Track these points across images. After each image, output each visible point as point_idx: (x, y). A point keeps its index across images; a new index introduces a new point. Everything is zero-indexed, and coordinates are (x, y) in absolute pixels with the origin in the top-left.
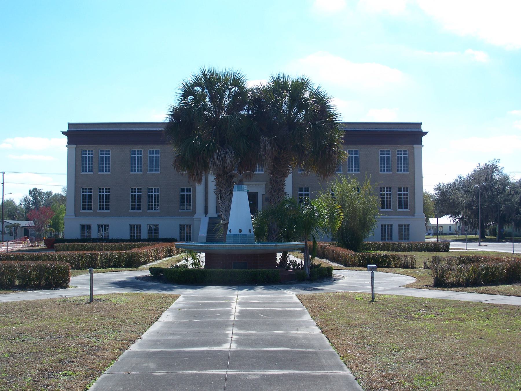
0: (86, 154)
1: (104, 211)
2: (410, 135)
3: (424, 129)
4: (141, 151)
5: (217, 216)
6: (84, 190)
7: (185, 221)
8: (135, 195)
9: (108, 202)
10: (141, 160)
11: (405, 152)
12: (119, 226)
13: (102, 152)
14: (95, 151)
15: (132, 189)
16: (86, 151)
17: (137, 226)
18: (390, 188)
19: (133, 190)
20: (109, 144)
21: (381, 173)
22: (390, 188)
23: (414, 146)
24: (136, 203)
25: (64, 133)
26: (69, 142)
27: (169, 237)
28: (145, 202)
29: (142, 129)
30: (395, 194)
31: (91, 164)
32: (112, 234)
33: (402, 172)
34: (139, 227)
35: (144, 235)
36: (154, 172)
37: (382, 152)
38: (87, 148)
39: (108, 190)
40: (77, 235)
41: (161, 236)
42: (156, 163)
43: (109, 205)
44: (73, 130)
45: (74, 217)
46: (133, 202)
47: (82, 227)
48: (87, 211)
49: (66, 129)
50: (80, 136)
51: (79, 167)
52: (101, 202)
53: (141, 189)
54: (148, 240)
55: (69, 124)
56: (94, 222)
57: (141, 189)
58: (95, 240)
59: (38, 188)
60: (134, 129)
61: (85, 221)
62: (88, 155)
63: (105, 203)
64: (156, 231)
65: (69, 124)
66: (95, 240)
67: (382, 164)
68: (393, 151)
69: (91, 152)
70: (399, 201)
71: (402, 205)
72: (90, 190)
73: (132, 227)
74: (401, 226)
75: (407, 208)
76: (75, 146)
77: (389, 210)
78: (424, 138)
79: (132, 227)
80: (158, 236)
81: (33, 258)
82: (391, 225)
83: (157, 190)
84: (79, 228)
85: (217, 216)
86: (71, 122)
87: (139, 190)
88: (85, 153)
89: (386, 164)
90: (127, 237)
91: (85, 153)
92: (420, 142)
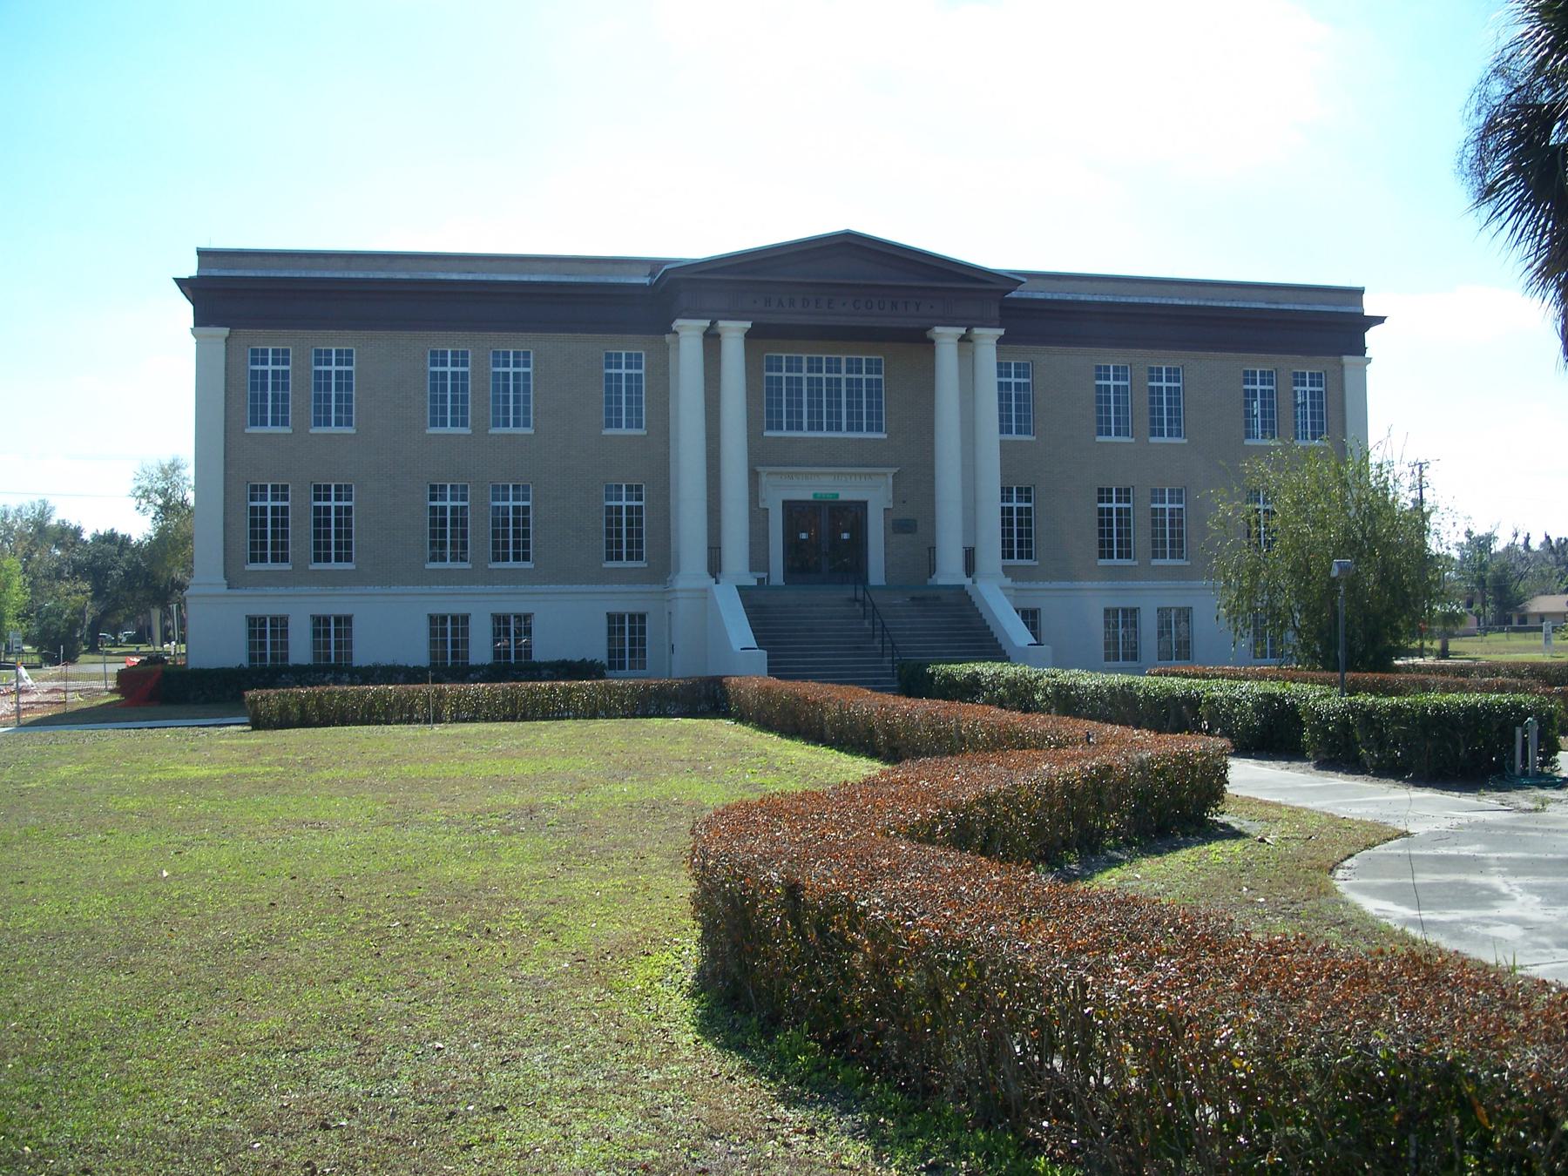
0: (444, 364)
1: (333, 565)
3: (1370, 308)
4: (465, 354)
5: (755, 583)
6: (257, 491)
7: (626, 600)
8: (1110, 510)
10: (286, 386)
11: (1316, 379)
12: (390, 624)
13: (323, 357)
14: (299, 352)
15: (317, 488)
16: (265, 352)
17: (454, 619)
18: (1127, 491)
19: (1104, 494)
20: (534, 330)
21: (1153, 440)
22: (1127, 491)
23: (1346, 359)
24: (446, 534)
25: (1380, 320)
26: (201, 320)
27: (576, 657)
28: (301, 535)
29: (470, 277)
31: (281, 400)
32: (544, 648)
33: (1113, 439)
34: (461, 621)
35: (481, 651)
36: (511, 430)
37: (438, 358)
38: (269, 340)
40: (418, 653)
41: (363, 655)
43: (349, 546)
44: (215, 273)
45: (224, 589)
46: (612, 533)
47: (256, 625)
48: (270, 566)
49: (190, 269)
50: (231, 294)
51: (241, 406)
53: (285, 488)
54: (493, 673)
55: (202, 253)
56: (480, 606)
57: (285, 488)
58: (303, 675)
60: (441, 276)
61: (267, 604)
62: (270, 367)
63: (333, 538)
64: (345, 642)
65: (202, 253)
66: (303, 675)
67: (438, 399)
68: (1287, 370)
69: (281, 357)
70: (285, 534)
71: (1111, 544)
72: (281, 492)
73: (437, 621)
74: (501, 622)
75: (1128, 556)
76: (225, 331)
77: (459, 565)
78: (1372, 336)
79: (437, 621)
80: (285, 657)
82: (465, 618)
83: (343, 492)
84: (242, 630)
85: (755, 583)
86: (206, 244)
88: (259, 356)
90: (418, 653)
91: (259, 356)
92: (1360, 349)
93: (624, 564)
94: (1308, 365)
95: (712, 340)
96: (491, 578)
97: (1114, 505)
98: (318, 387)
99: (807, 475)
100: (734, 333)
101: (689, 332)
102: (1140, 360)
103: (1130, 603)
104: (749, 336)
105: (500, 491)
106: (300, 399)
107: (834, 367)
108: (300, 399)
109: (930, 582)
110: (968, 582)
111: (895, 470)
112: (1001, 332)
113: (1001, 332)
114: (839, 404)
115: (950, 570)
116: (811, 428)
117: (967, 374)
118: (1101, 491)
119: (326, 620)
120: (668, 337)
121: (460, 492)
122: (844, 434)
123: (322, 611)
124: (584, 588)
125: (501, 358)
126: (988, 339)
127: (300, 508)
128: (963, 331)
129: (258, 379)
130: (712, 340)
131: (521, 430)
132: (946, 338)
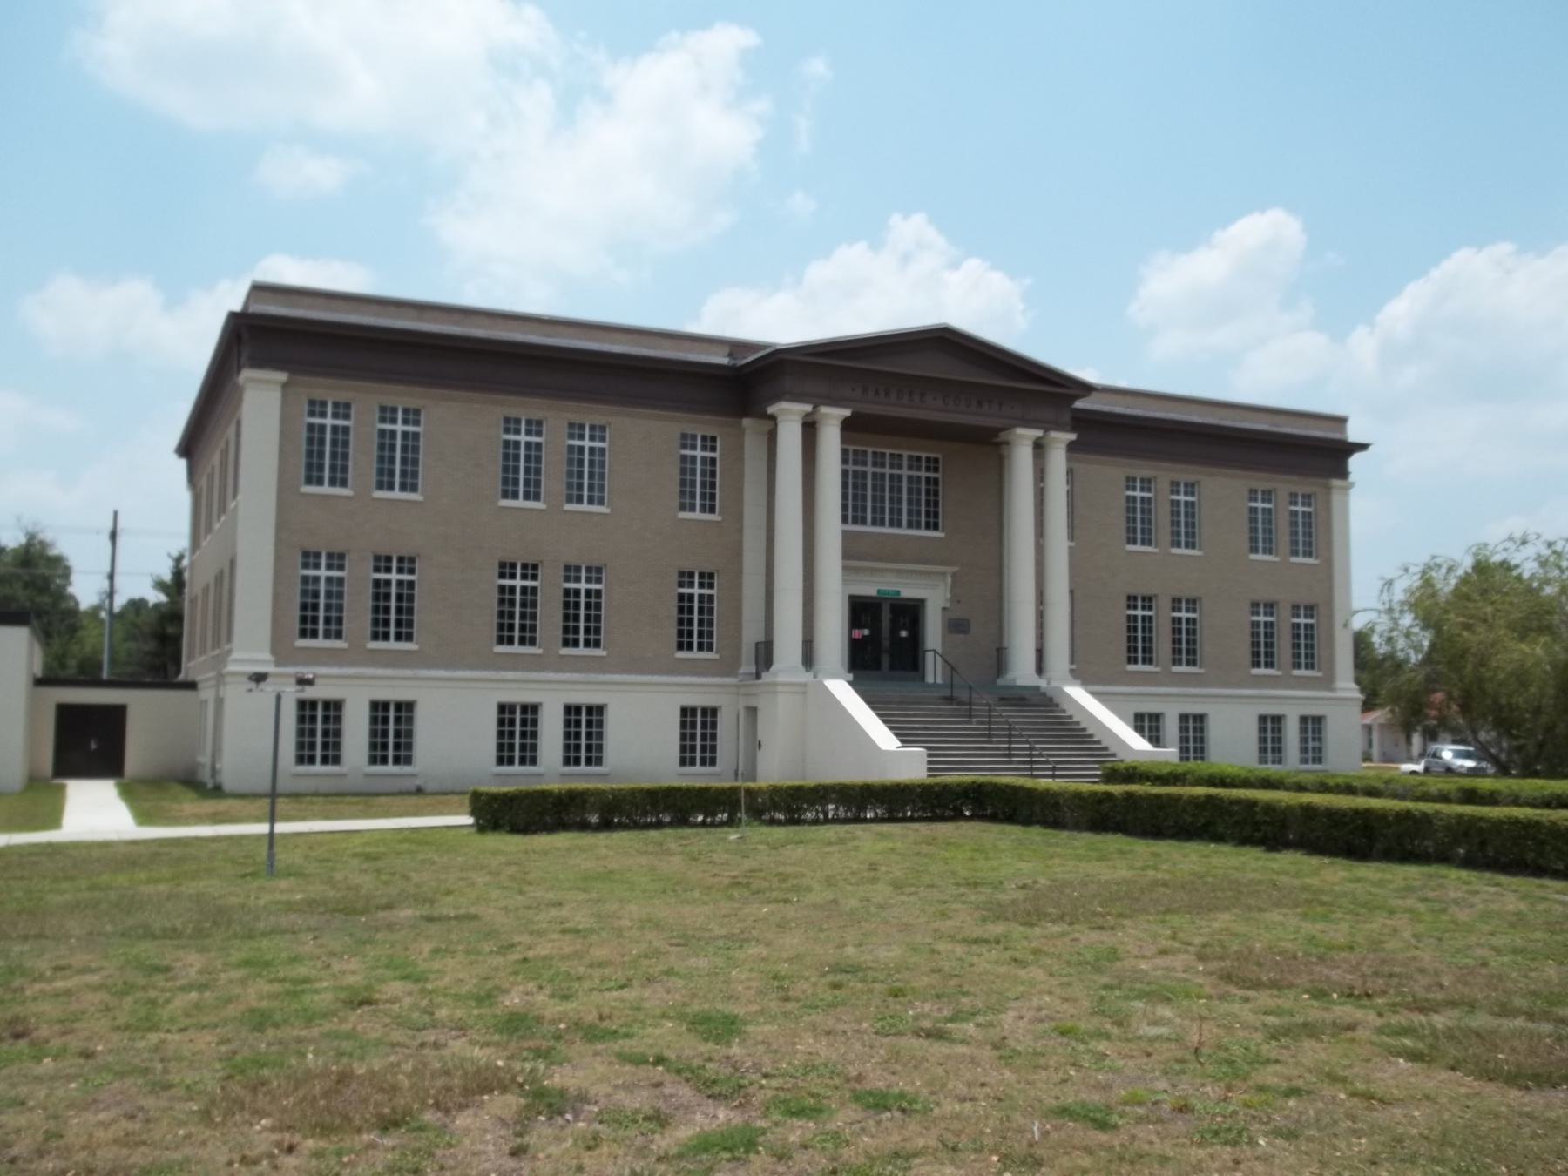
2: (1310, 453)
3: (1353, 434)
6: (310, 558)
8: (691, 597)
9: (406, 610)
13: (387, 414)
14: (365, 409)
19: (507, 569)
23: (746, 422)
24: (514, 622)
25: (1363, 447)
30: (1163, 617)
31: (534, 471)
34: (531, 710)
37: (511, 424)
38: (330, 390)
39: (407, 564)
42: (591, 475)
52: (379, 610)
59: (47, 536)
65: (259, 290)
67: (509, 469)
69: (343, 410)
73: (505, 711)
76: (282, 377)
77: (404, 646)
78: (1355, 462)
81: (1257, 826)
83: (595, 573)
84: (561, 711)
87: (531, 570)
89: (1260, 534)
91: (317, 407)
92: (1343, 474)
93: (695, 654)
94: (1302, 486)
95: (810, 429)
96: (376, 659)
97: (583, 586)
98: (310, 441)
99: (873, 571)
100: (832, 419)
101: (790, 416)
102: (1164, 474)
103: (594, 699)
104: (847, 426)
105: (571, 572)
106: (362, 460)
107: (896, 461)
108: (362, 460)
109: (1000, 682)
110: (1042, 683)
111: (955, 569)
112: (1073, 437)
113: (1073, 437)
114: (864, 498)
115: (1022, 672)
116: (874, 523)
117: (1039, 477)
118: (567, 568)
119: (578, 709)
120: (1336, 482)
121: (337, 560)
122: (904, 531)
123: (383, 694)
124: (656, 679)
125: (576, 430)
126: (1061, 440)
127: (359, 580)
128: (808, 408)
129: (315, 432)
130: (810, 429)
131: (595, 508)
132: (1023, 438)
